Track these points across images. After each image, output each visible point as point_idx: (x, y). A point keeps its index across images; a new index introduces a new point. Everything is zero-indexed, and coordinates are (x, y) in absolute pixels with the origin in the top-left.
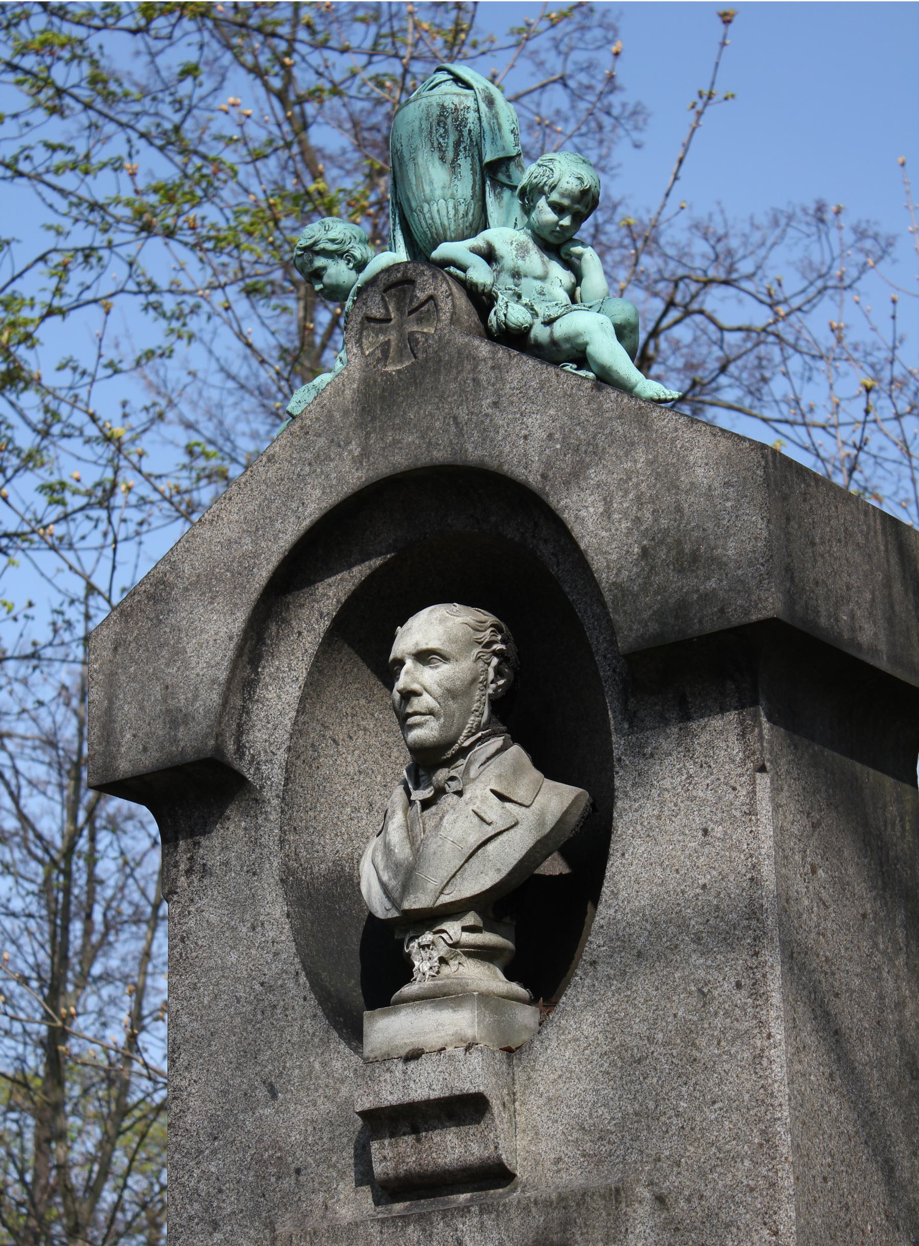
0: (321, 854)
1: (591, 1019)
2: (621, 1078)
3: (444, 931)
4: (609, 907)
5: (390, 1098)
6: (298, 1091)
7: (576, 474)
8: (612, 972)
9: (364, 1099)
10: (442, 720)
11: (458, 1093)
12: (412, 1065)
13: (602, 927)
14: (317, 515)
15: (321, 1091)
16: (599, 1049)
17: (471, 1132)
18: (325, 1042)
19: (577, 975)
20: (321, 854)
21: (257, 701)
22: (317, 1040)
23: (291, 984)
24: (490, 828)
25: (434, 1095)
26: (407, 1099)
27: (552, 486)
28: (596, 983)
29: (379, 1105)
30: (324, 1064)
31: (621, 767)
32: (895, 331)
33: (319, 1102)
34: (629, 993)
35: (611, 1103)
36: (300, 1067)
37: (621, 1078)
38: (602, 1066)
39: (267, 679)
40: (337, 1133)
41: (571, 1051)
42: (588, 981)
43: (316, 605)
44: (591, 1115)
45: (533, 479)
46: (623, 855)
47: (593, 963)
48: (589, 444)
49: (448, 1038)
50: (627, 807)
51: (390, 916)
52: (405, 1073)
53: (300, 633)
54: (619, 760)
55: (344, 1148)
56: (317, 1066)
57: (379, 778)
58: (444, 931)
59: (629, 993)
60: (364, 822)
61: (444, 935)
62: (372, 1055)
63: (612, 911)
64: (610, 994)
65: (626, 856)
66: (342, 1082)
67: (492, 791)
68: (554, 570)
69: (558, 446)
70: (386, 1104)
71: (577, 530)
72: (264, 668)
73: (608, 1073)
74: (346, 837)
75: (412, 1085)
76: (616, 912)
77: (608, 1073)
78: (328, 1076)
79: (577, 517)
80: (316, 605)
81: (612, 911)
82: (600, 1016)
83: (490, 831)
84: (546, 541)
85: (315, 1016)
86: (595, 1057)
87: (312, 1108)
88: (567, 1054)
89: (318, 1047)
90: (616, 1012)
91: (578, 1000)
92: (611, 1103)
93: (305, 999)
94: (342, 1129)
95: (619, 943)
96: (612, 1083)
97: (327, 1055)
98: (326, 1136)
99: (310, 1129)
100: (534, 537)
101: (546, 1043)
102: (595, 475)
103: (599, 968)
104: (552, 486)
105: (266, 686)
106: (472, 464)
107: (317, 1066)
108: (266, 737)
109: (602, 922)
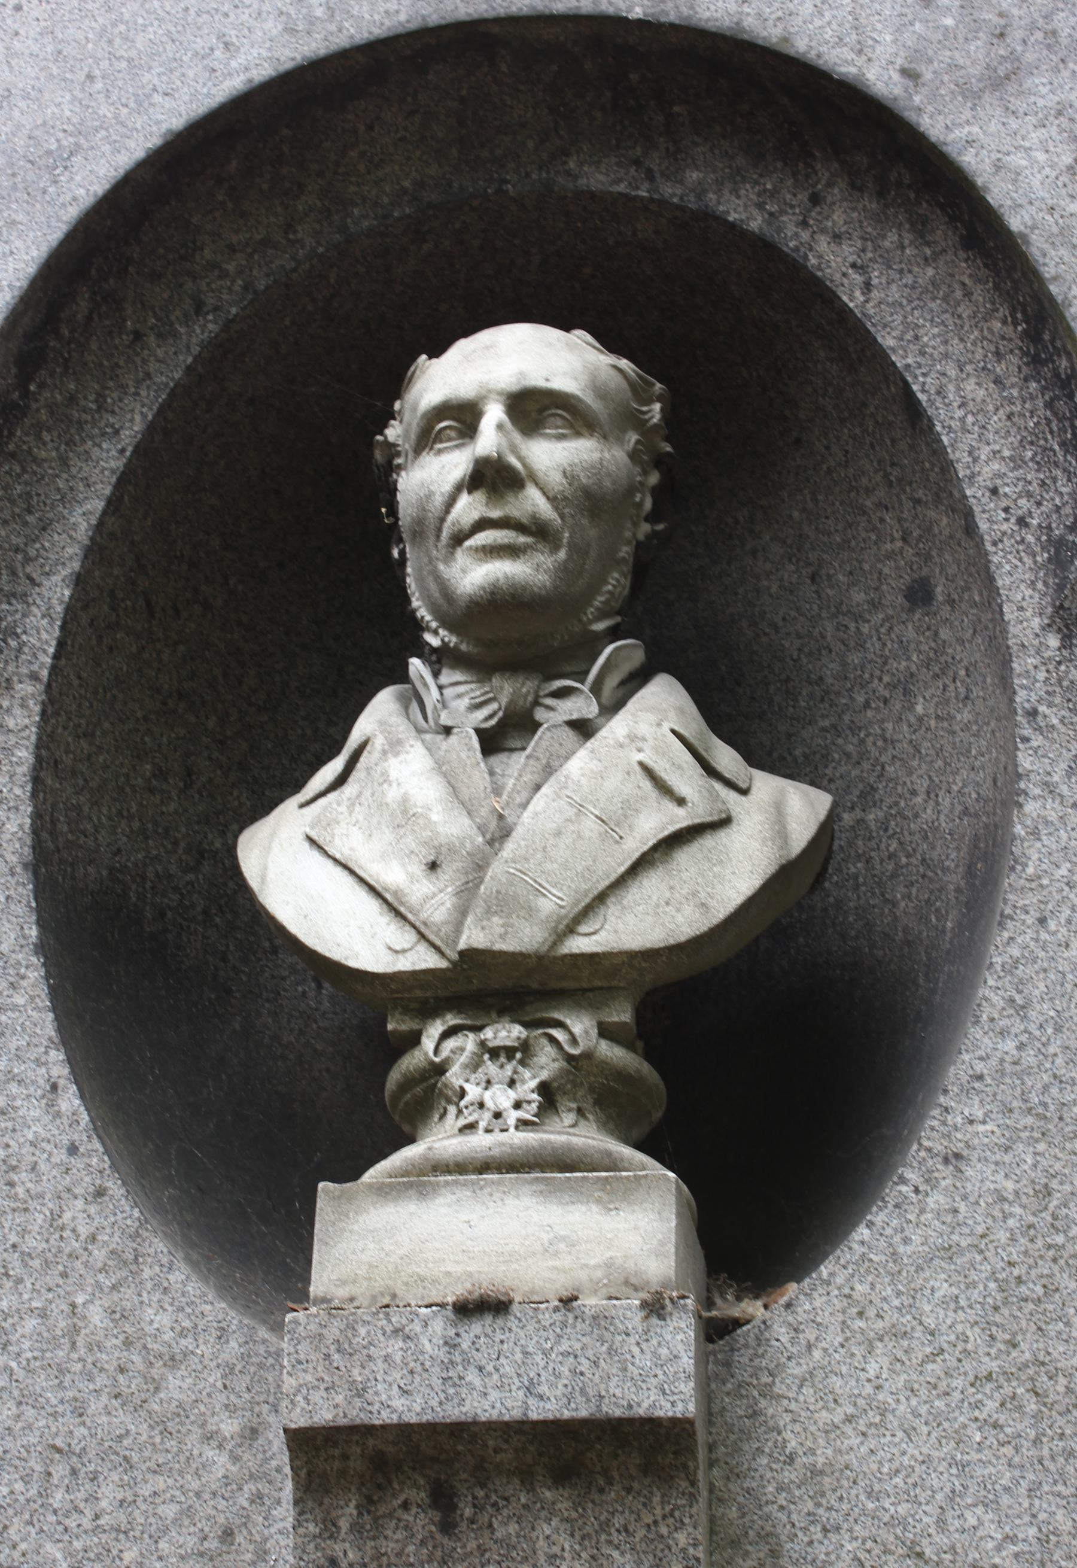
0: (91, 842)
1: (944, 1289)
2: (1037, 1442)
3: (560, 1025)
4: (1003, 1033)
5: (398, 1403)
6: (29, 1371)
7: (1001, 80)
8: (1010, 1185)
9: (316, 1396)
10: (562, 554)
11: (618, 1413)
12: (477, 1327)
13: (980, 1077)
14: (263, 72)
15: (101, 1380)
16: (967, 1365)
17: (618, 1521)
18: (129, 1263)
19: (903, 1180)
20: (91, 842)
21: (13, 455)
22: (99, 1255)
23: (33, 1111)
24: (681, 812)
25: (537, 1412)
26: (453, 1413)
27: (934, 96)
28: (962, 1207)
29: (363, 1418)
30: (118, 1315)
31: (1039, 729)
32: (537, 484)
33: (95, 1406)
34: (1060, 1239)
35: (1005, 1500)
36: (43, 1314)
37: (1037, 1442)
38: (978, 1405)
39: (44, 415)
40: (145, 1491)
41: (885, 1362)
42: (936, 1200)
43: (189, 285)
44: (941, 1524)
45: (880, 78)
46: (1042, 921)
47: (954, 1159)
48: (1033, 28)
49: (583, 1275)
50: (1053, 817)
51: (404, 964)
52: (451, 1345)
53: (138, 336)
54: (1033, 713)
55: (166, 1530)
56: (96, 1316)
57: (212, 723)
58: (560, 1025)
59: (1060, 1239)
60: (172, 807)
61: (559, 1034)
62: (342, 1293)
63: (1010, 1045)
64: (1003, 1236)
65: (1052, 925)
66: (173, 1362)
67: (673, 731)
68: (853, 299)
69: (949, 22)
70: (386, 1417)
71: (998, 194)
72: (42, 386)
73: (996, 1426)
74: (136, 825)
75: (472, 1376)
76: (1021, 1047)
77: (996, 1426)
78: (128, 1343)
79: (998, 166)
80: (189, 285)
81: (1010, 1045)
82: (974, 1285)
83: (681, 818)
84: (837, 238)
85: (100, 1193)
86: (958, 1383)
87: (72, 1420)
88: (872, 1369)
89: (104, 1269)
90: (1019, 1280)
91: (906, 1241)
92: (1005, 1500)
93: (73, 1150)
94: (160, 1483)
95: (1030, 1120)
96: (1008, 1450)
97: (128, 1292)
98: (109, 1494)
99: (60, 1471)
100: (804, 224)
101: (810, 1334)
102: (1043, 90)
103: (969, 1172)
104: (934, 96)
105: (38, 428)
106: (711, 26)
107: (96, 1316)
108: (19, 541)
109: (979, 1067)
